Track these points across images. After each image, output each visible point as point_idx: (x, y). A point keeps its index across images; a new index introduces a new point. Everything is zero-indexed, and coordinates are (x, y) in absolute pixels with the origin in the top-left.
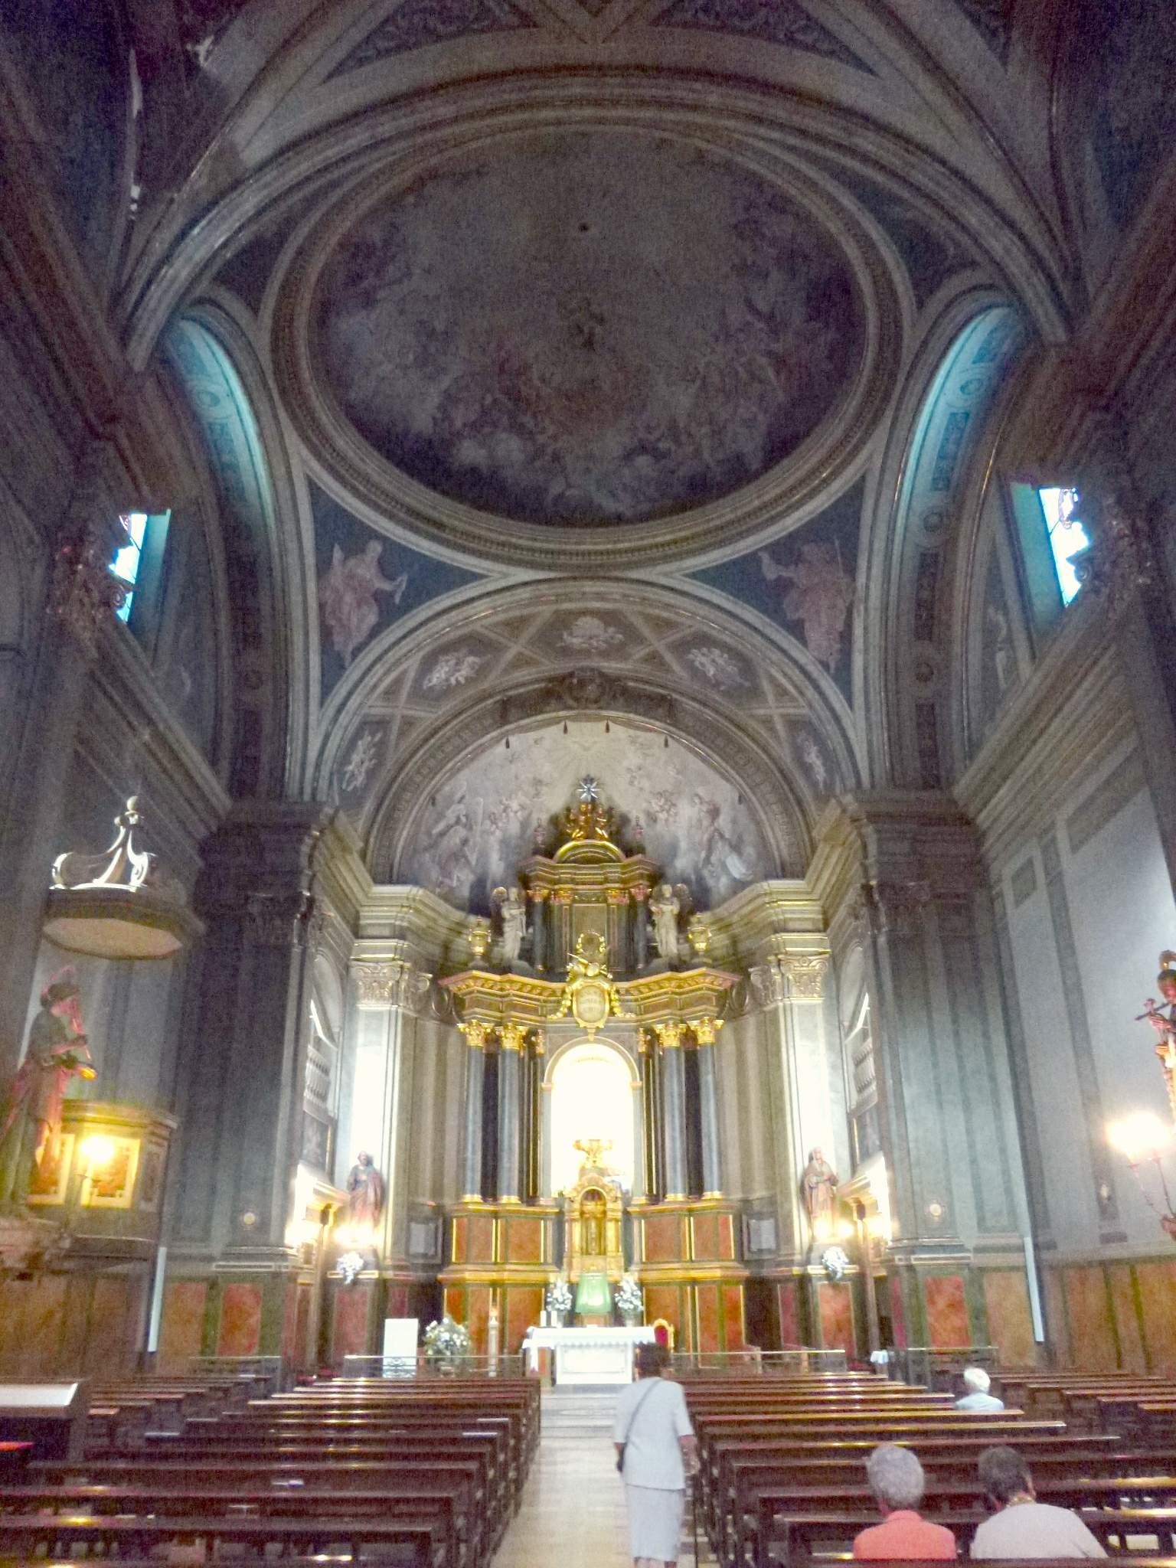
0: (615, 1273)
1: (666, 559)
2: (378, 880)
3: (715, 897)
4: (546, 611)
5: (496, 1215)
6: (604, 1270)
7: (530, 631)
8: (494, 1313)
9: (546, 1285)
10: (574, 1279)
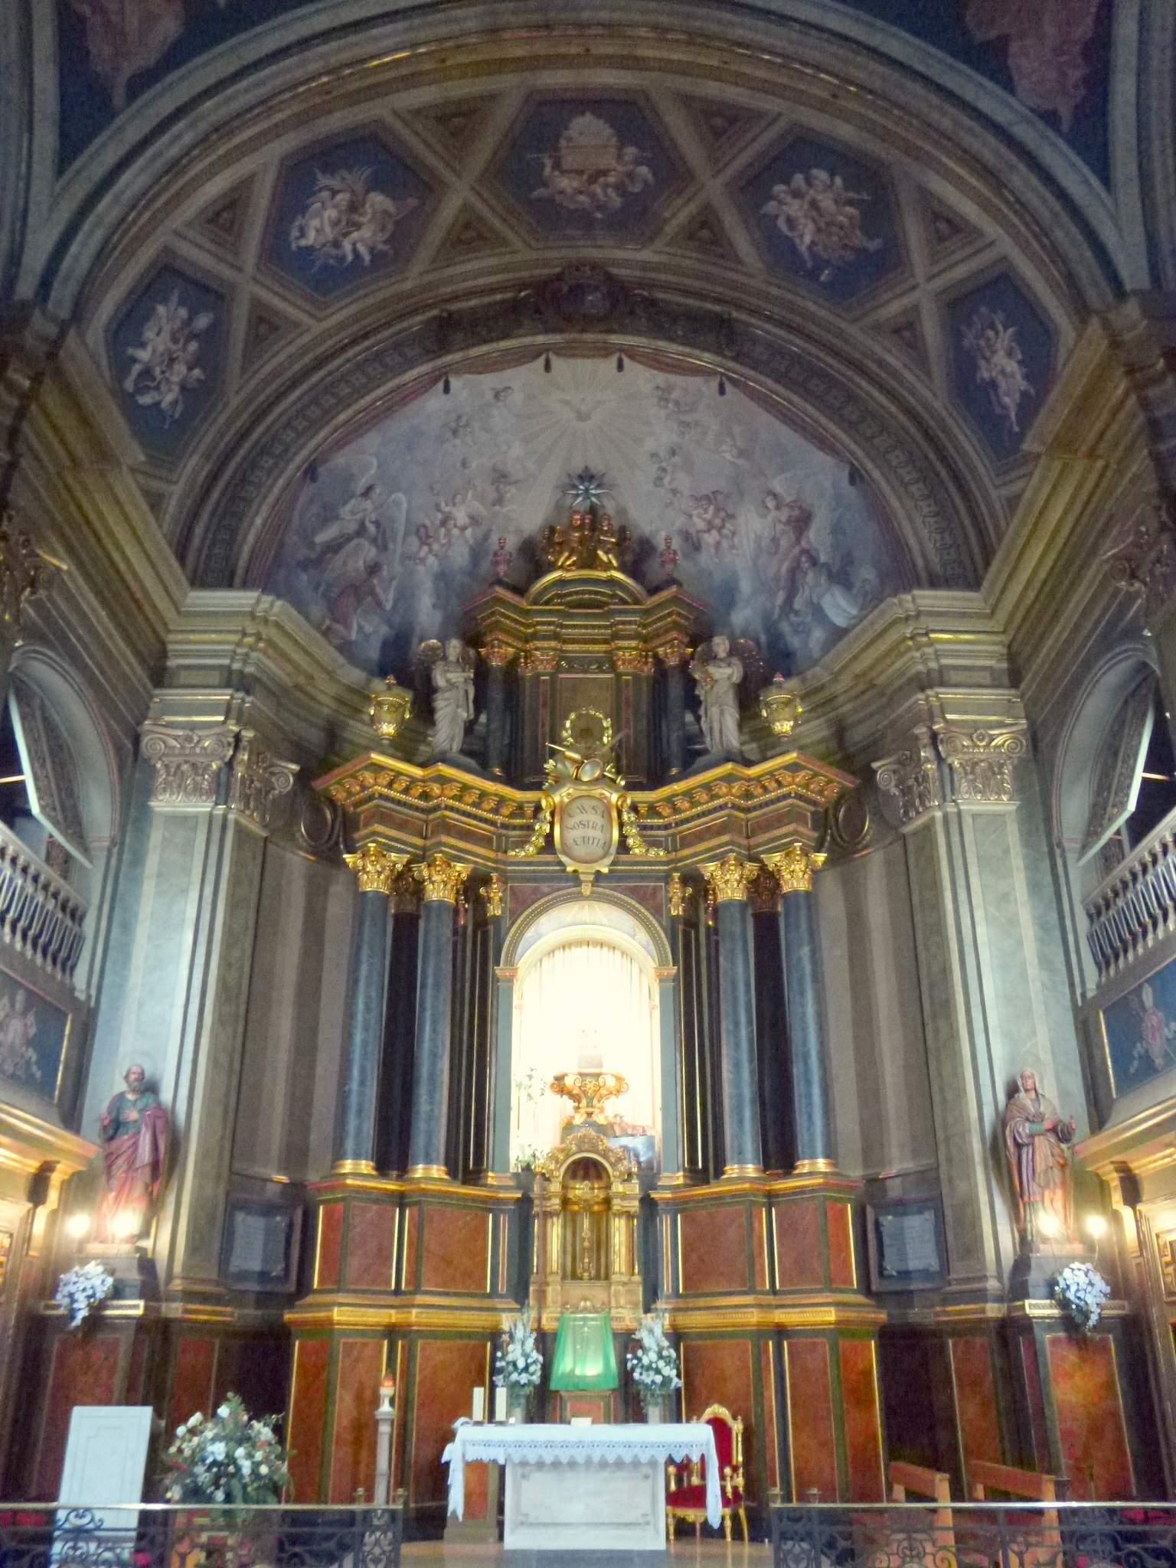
0: (627, 1316)
2: (199, 580)
5: (401, 1200)
6: (607, 1306)
8: (387, 1390)
9: (495, 1336)
10: (547, 1324)
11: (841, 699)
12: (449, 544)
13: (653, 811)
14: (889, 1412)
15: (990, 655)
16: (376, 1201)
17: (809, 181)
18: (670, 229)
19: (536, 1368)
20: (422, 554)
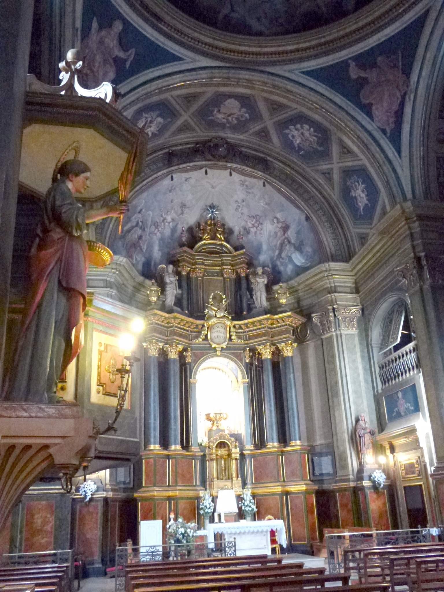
1: (291, 61)
3: (284, 276)
4: (210, 91)
7: (196, 106)
9: (198, 498)
10: (214, 494)
11: (300, 291)
12: (165, 228)
13: (240, 327)
14: (319, 515)
15: (350, 282)
16: (162, 458)
17: (302, 127)
18: (251, 131)
19: (212, 508)
20: (156, 232)
